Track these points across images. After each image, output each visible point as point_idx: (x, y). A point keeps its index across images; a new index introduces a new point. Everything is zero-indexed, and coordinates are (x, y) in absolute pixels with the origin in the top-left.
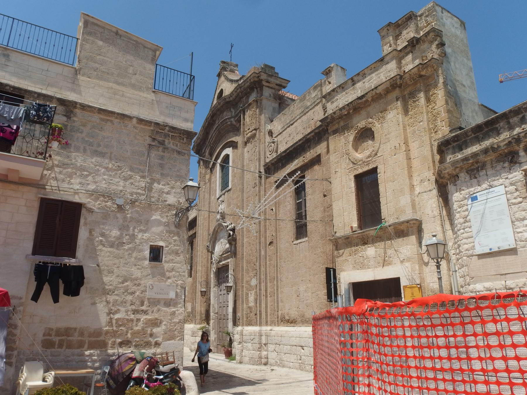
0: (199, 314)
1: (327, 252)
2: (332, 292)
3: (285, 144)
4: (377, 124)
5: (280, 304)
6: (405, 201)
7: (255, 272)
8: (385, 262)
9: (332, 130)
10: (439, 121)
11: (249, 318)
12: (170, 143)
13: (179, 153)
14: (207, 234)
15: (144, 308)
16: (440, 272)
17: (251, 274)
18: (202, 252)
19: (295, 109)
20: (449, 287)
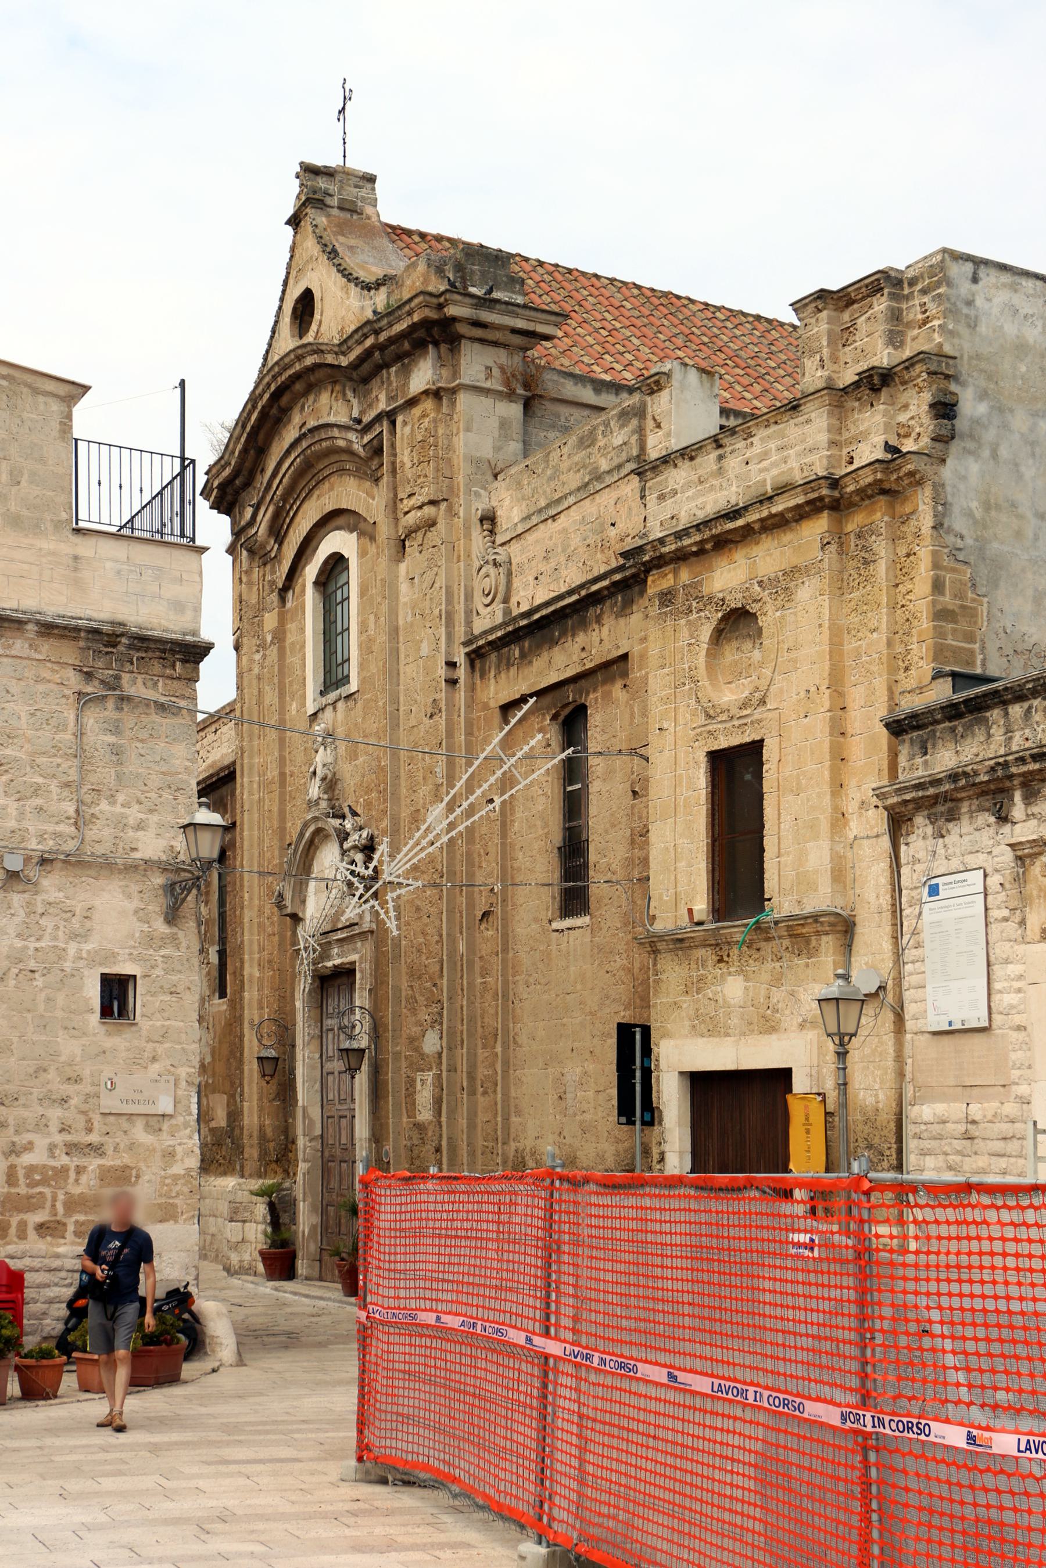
0: (255, 1141)
1: (636, 971)
2: (635, 1100)
3: (531, 578)
4: (769, 608)
5: (514, 1119)
6: (818, 856)
7: (435, 1008)
8: (767, 1024)
9: (657, 589)
10: (915, 639)
11: (417, 1162)
12: (135, 686)
13: (161, 707)
14: (276, 843)
15: (94, 1138)
16: (844, 1069)
17: (424, 1015)
18: (260, 911)
19: (565, 465)
20: (894, 1105)
